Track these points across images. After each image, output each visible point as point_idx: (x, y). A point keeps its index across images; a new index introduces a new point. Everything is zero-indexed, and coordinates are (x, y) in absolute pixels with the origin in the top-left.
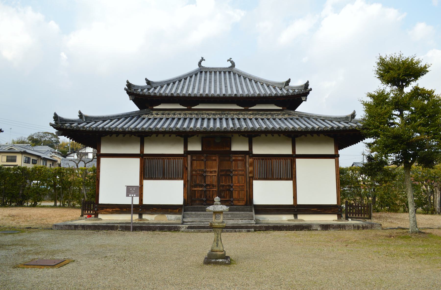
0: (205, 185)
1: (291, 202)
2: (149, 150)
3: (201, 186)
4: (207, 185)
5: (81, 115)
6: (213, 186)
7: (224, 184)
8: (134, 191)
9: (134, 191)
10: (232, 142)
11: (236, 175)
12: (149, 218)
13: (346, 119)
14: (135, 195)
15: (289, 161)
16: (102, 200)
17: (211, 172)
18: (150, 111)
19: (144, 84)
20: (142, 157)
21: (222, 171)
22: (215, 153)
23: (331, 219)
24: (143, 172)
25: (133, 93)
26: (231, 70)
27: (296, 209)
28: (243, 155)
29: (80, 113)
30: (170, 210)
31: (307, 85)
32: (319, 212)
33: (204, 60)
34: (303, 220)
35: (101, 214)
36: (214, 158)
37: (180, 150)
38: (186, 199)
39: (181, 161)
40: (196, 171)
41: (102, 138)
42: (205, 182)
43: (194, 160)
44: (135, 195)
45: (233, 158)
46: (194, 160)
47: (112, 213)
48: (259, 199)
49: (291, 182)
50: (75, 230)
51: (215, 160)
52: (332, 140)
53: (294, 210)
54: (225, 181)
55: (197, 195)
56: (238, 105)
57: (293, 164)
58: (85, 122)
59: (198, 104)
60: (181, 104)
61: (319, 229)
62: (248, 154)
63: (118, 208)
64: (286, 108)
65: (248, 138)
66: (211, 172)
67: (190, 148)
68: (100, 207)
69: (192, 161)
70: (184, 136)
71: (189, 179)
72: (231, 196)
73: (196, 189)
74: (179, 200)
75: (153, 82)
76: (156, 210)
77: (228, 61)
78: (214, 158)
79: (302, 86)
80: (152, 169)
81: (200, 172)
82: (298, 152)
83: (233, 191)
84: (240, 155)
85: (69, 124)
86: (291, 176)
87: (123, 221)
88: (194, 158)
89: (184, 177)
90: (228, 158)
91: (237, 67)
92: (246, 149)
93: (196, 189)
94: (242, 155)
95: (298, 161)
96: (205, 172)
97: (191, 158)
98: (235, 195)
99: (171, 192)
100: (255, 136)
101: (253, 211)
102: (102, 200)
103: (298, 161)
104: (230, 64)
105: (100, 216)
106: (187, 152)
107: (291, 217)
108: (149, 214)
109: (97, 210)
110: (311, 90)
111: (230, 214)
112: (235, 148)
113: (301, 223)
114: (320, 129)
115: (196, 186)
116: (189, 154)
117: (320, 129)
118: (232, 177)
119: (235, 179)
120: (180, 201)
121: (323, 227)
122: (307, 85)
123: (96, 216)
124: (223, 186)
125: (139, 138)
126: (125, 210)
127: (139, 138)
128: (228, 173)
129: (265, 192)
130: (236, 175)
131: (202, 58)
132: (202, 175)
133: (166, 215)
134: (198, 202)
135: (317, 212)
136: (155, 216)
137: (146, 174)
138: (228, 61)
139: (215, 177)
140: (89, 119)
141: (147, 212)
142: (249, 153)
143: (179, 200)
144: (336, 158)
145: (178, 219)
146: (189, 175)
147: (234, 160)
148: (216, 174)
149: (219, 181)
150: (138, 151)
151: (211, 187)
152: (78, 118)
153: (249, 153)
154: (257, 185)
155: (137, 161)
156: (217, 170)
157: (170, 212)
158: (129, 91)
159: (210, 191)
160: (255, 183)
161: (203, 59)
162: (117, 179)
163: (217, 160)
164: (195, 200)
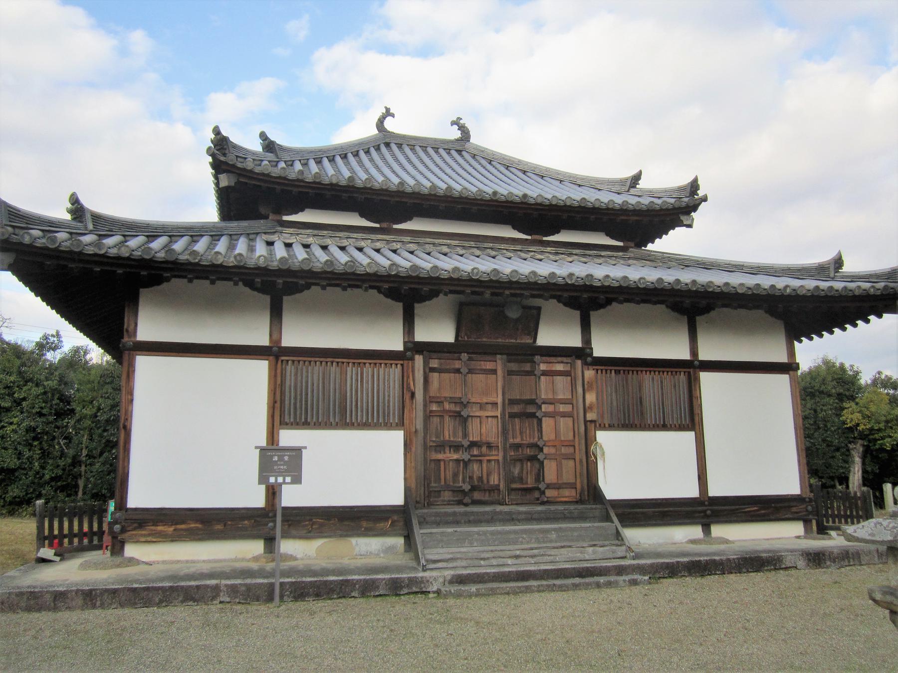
0: (466, 443)
1: (693, 492)
2: (299, 334)
3: (457, 447)
4: (473, 444)
5: (78, 210)
6: (489, 446)
7: (518, 440)
8: (286, 463)
9: (286, 463)
10: (542, 316)
11: (547, 415)
12: (300, 551)
13: (820, 271)
14: (288, 479)
15: (683, 378)
16: (141, 494)
17: (482, 406)
18: (274, 227)
19: (255, 146)
20: (277, 357)
21: (512, 402)
22: (490, 351)
23: (786, 534)
24: (278, 405)
25: (234, 166)
26: (461, 146)
27: (707, 510)
28: (569, 360)
29: (75, 200)
30: (364, 524)
31: (694, 186)
32: (764, 515)
33: (393, 116)
34: (727, 541)
35: (137, 542)
36: (489, 366)
37: (390, 339)
38: (413, 486)
39: (395, 372)
40: (439, 403)
41: (144, 293)
42: (465, 435)
43: (433, 370)
44: (288, 479)
45: (543, 367)
46: (433, 370)
47: (175, 538)
48: (615, 485)
49: (690, 436)
50: (55, 609)
51: (494, 372)
52: (780, 325)
53: (705, 511)
54: (521, 433)
55: (446, 474)
56: (514, 228)
57: (693, 386)
58: (91, 232)
59: (410, 219)
60: (362, 215)
61: (801, 563)
62: (578, 357)
63: (197, 521)
64: (633, 245)
65: (578, 313)
66: (482, 406)
67: (425, 333)
68: (135, 521)
69: (429, 370)
70: (407, 294)
71: (419, 425)
72: (540, 476)
73: (440, 456)
74: (390, 491)
75: (282, 148)
76: (322, 525)
77: (453, 123)
78: (489, 366)
79: (681, 189)
80: (306, 394)
81: (452, 407)
82: (705, 355)
83: (546, 462)
84: (560, 359)
85: (40, 233)
86: (690, 419)
87: (218, 567)
88: (434, 364)
89: (406, 422)
90: (527, 367)
91: (476, 139)
92: (574, 340)
93: (440, 456)
94: (565, 360)
95: (705, 378)
96: (465, 406)
97: (426, 363)
98: (550, 473)
99: (362, 466)
100: (600, 305)
101: (615, 519)
102: (141, 494)
103: (705, 378)
104: (455, 134)
105: (131, 550)
106: (414, 348)
107: (696, 532)
108: (301, 538)
109: (123, 530)
110: (704, 199)
111: (555, 530)
112: (547, 337)
113: (722, 547)
114: (788, 290)
115: (441, 447)
116: (420, 352)
117: (788, 290)
118: (540, 421)
119: (547, 423)
120: (394, 496)
121: (809, 560)
122: (694, 186)
123: (117, 548)
124: (517, 446)
125: (267, 299)
126: (219, 527)
127: (267, 299)
128: (531, 409)
129: (636, 463)
130: (547, 415)
131: (388, 110)
132: (457, 415)
133: (354, 540)
134: (447, 495)
135: (759, 516)
136: (318, 543)
137: (288, 408)
138: (453, 123)
139: (495, 420)
140: (105, 225)
141: (294, 532)
142: (582, 354)
143: (390, 491)
144: (791, 372)
145: (390, 550)
146: (420, 414)
147: (545, 373)
148: (498, 413)
149: (505, 432)
150: (262, 339)
151: (484, 449)
152: (68, 217)
153: (582, 354)
154: (612, 444)
155: (260, 368)
156: (500, 400)
157: (367, 529)
158: (222, 159)
159: (481, 461)
160: (603, 437)
161: (388, 113)
162: (194, 426)
163: (500, 372)
164: (438, 493)
